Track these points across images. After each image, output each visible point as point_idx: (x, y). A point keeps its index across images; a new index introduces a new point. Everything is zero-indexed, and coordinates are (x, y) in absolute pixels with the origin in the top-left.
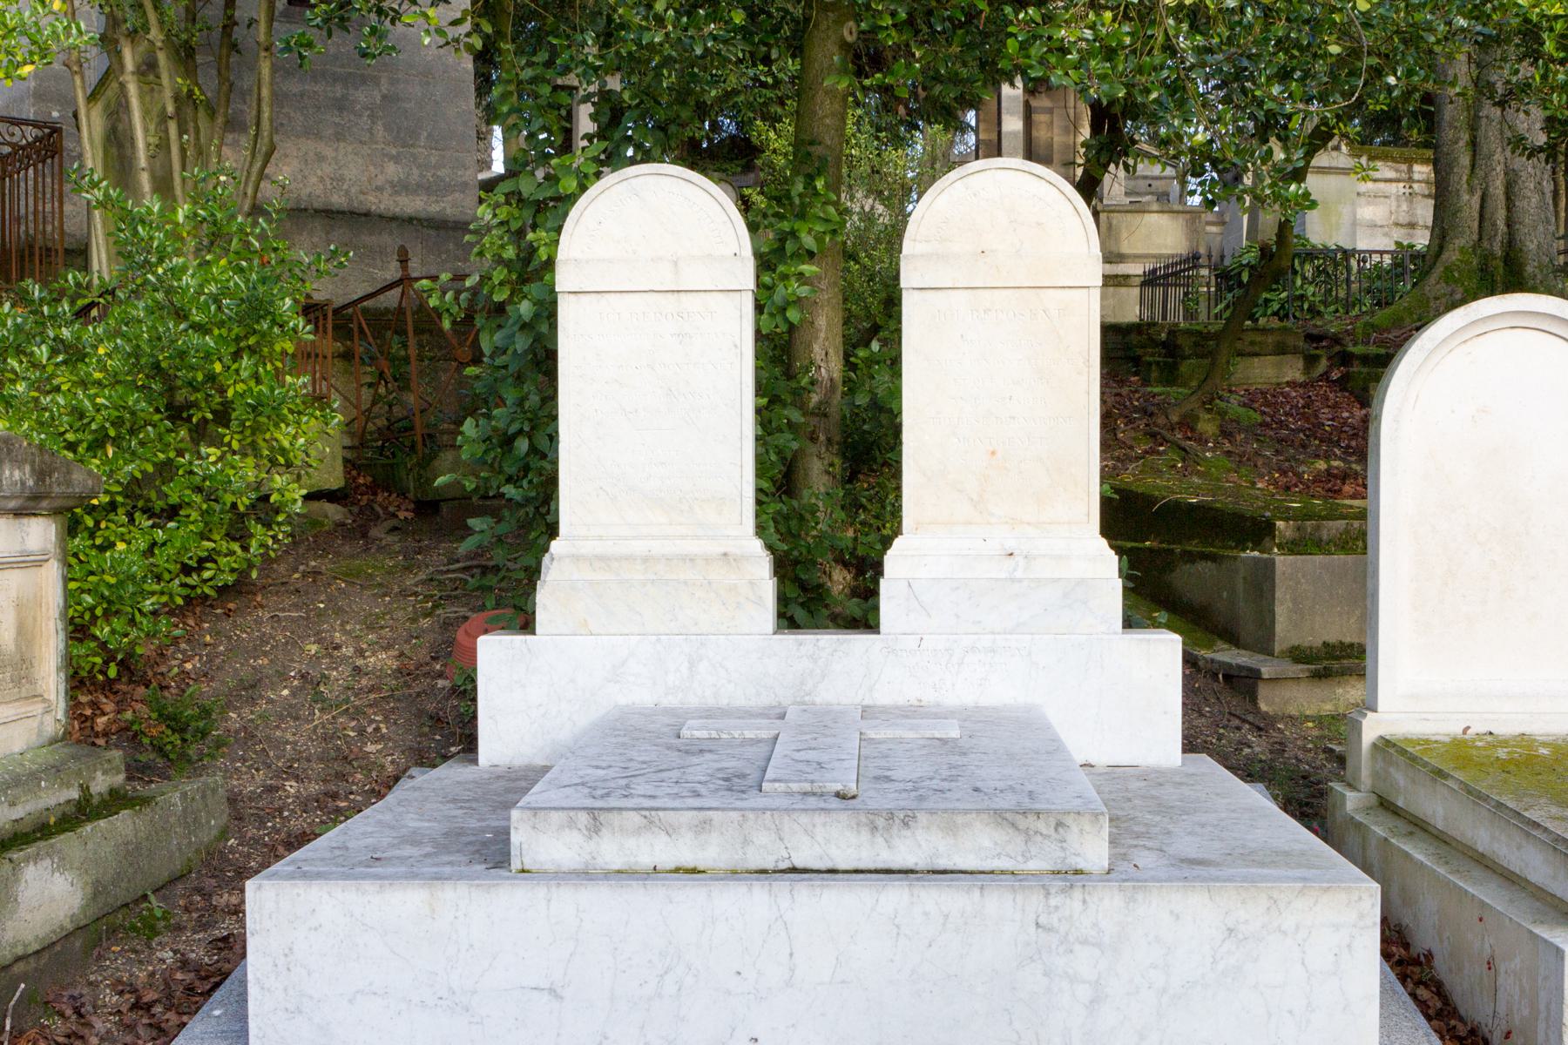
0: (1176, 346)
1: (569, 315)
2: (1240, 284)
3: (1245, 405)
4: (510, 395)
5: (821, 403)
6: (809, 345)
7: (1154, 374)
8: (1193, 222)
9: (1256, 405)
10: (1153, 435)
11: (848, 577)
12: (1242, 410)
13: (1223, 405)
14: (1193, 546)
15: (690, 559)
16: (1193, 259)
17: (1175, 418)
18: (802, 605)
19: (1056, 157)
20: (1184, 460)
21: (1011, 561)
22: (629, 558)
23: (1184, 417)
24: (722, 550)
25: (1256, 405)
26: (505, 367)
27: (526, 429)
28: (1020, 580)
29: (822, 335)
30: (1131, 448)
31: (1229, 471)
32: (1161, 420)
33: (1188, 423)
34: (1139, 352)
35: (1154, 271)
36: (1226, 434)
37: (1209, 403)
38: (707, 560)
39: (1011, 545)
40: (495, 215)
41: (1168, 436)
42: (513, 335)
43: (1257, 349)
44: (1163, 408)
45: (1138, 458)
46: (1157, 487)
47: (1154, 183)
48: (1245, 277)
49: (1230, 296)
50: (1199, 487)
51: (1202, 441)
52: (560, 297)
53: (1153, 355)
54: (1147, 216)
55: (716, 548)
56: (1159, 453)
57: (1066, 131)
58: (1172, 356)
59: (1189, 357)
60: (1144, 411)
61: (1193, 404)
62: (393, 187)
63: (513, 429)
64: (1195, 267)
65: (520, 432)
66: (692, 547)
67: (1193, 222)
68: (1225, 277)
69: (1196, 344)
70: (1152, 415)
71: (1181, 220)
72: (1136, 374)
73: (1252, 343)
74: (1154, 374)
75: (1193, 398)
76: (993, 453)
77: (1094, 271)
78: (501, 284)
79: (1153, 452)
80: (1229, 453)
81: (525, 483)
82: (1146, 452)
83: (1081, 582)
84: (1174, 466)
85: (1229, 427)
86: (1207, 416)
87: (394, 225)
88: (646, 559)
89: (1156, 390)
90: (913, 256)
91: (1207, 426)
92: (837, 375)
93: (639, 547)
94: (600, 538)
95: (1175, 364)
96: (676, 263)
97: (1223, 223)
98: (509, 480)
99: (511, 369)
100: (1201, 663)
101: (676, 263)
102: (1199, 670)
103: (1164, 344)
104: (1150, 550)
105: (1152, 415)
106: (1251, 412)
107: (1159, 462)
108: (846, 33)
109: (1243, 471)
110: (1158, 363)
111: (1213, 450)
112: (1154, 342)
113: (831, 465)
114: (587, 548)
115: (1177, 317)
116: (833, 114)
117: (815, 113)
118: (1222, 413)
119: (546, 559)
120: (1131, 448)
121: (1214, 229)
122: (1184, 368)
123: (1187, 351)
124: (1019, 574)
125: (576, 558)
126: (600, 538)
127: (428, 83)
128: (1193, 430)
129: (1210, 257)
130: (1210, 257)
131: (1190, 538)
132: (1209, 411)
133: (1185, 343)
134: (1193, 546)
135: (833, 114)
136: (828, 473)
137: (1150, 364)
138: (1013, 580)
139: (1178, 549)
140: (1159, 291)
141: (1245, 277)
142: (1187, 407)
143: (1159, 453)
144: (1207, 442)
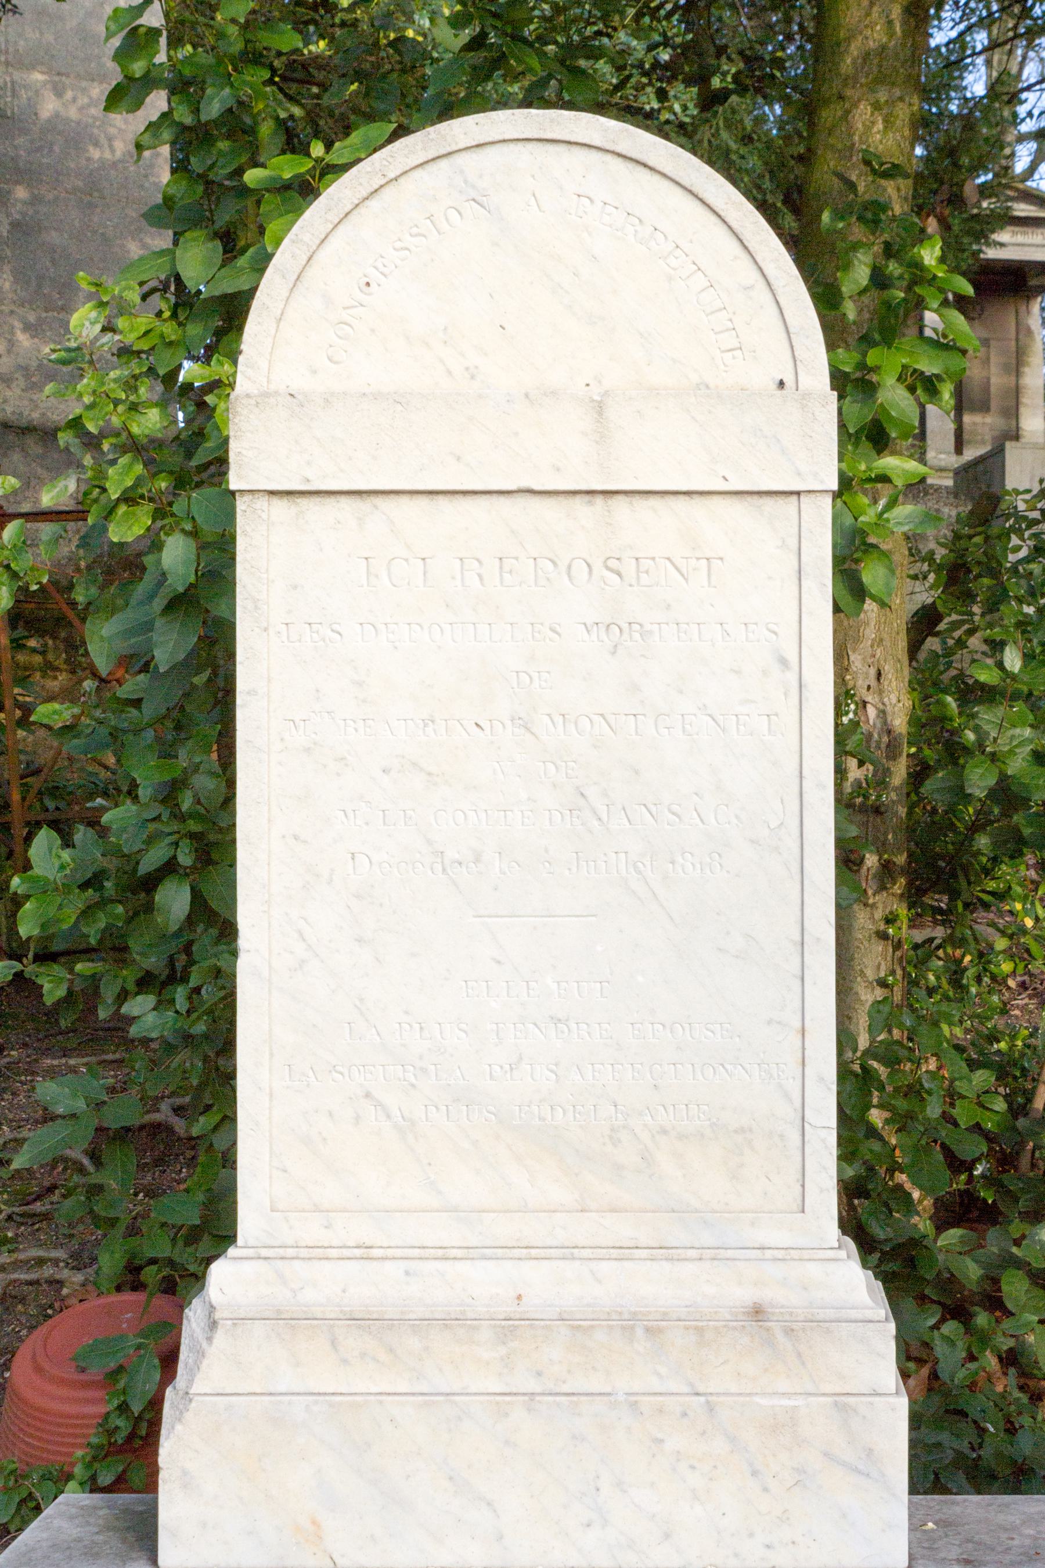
1: (264, 548)
4: (148, 776)
11: (158, 426)
15: (645, 1326)
19: (994, 404)
22: (454, 1322)
24: (745, 1295)
26: (137, 703)
27: (185, 859)
38: (701, 1327)
40: (109, 328)
42: (148, 627)
52: (241, 505)
55: (729, 1289)
57: (1006, 368)
62: (27, 376)
63: (151, 860)
65: (170, 868)
66: (652, 1286)
78: (129, 498)
81: (180, 994)
87: (30, 441)
88: (513, 1326)
92: (900, 723)
93: (485, 1284)
94: (365, 1253)
96: (599, 408)
98: (145, 982)
99: (149, 710)
101: (599, 408)
113: (890, 920)
114: (325, 1286)
119: (194, 1317)
125: (288, 1321)
126: (365, 1253)
127: (91, 206)
136: (883, 936)
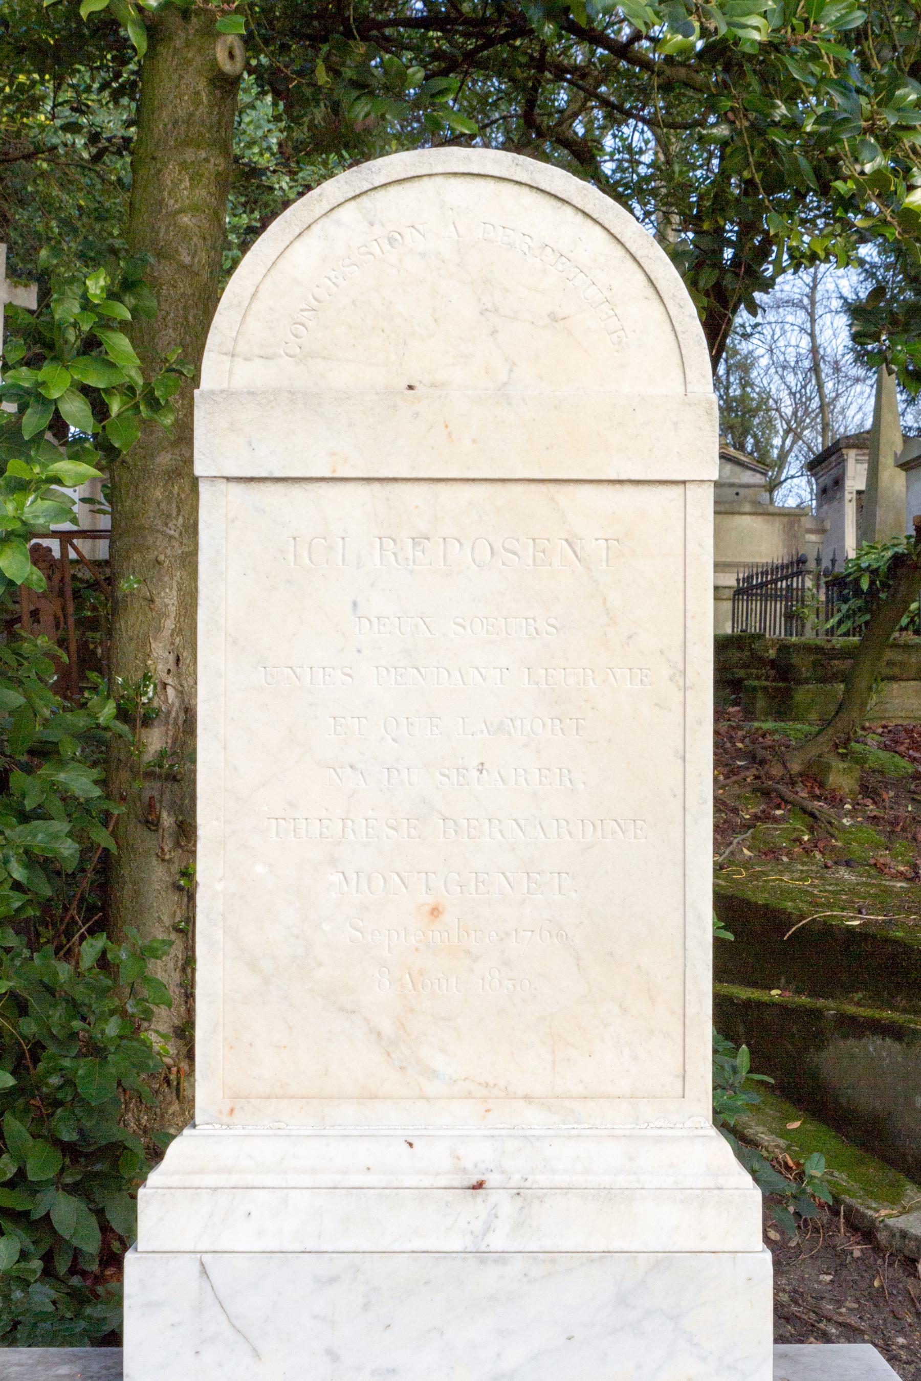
0: (790, 667)
2: (858, 592)
3: (886, 748)
5: (162, 754)
6: (144, 645)
7: (761, 703)
8: (791, 527)
9: (902, 748)
10: (766, 793)
12: (884, 755)
13: (857, 747)
14: (856, 1007)
16: (797, 566)
17: (796, 767)
18: (72, 1189)
20: (811, 830)
21: (478, 1204)
23: (809, 766)
25: (902, 748)
28: (502, 1257)
29: (169, 624)
30: (735, 811)
31: (877, 847)
32: (777, 770)
33: (814, 775)
34: (741, 673)
35: (750, 577)
36: (867, 790)
37: (843, 746)
39: (479, 1157)
41: (789, 796)
43: (897, 671)
44: (779, 752)
45: (746, 827)
46: (786, 893)
47: (742, 492)
48: (865, 585)
49: (845, 607)
50: (853, 892)
51: (835, 800)
53: (758, 678)
54: (737, 517)
56: (776, 820)
58: (784, 679)
59: (807, 681)
60: (752, 757)
61: (821, 747)
64: (799, 573)
67: (791, 527)
68: (840, 584)
69: (815, 664)
70: (762, 762)
71: (778, 523)
72: (735, 703)
73: (890, 663)
74: (761, 703)
75: (820, 739)
76: (435, 912)
77: (697, 448)
79: (766, 817)
80: (874, 819)
82: (756, 817)
83: (665, 1259)
84: (799, 840)
85: (873, 781)
86: (842, 765)
89: (769, 725)
90: (229, 394)
91: (842, 779)
95: (788, 690)
97: (823, 531)
100: (882, 1237)
102: (878, 1249)
103: (773, 663)
104: (782, 1007)
105: (762, 762)
106: (897, 758)
107: (777, 834)
108: (221, 56)
109: (898, 847)
110: (765, 689)
111: (851, 814)
112: (758, 660)
115: (776, 630)
116: (195, 209)
117: (161, 203)
118: (860, 760)
120: (735, 811)
121: (812, 537)
122: (801, 695)
123: (805, 673)
124: (497, 1241)
128: (821, 785)
129: (818, 561)
130: (818, 561)
131: (848, 989)
132: (843, 757)
133: (803, 664)
134: (856, 1007)
135: (195, 209)
137: (755, 689)
138: (481, 1255)
139: (830, 1006)
140: (756, 606)
141: (865, 585)
142: (813, 751)
143: (776, 820)
144: (842, 802)
